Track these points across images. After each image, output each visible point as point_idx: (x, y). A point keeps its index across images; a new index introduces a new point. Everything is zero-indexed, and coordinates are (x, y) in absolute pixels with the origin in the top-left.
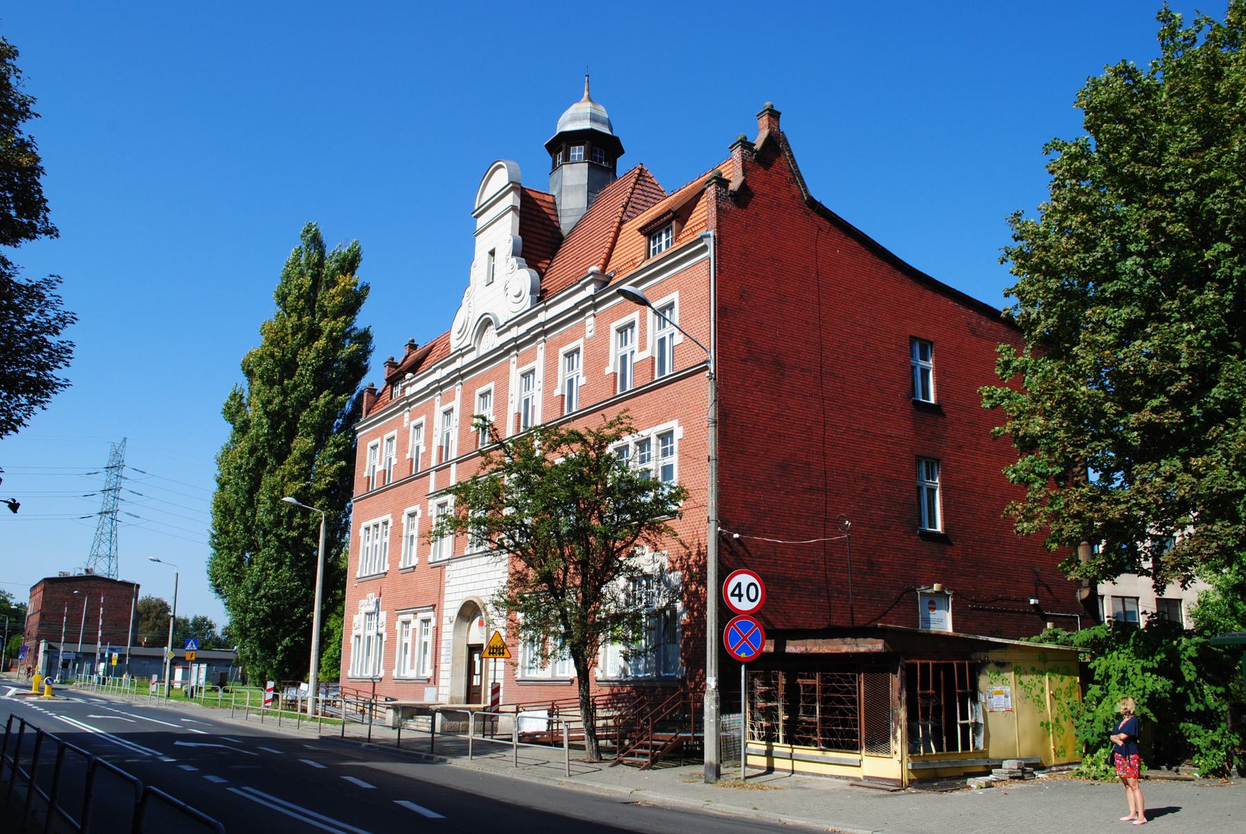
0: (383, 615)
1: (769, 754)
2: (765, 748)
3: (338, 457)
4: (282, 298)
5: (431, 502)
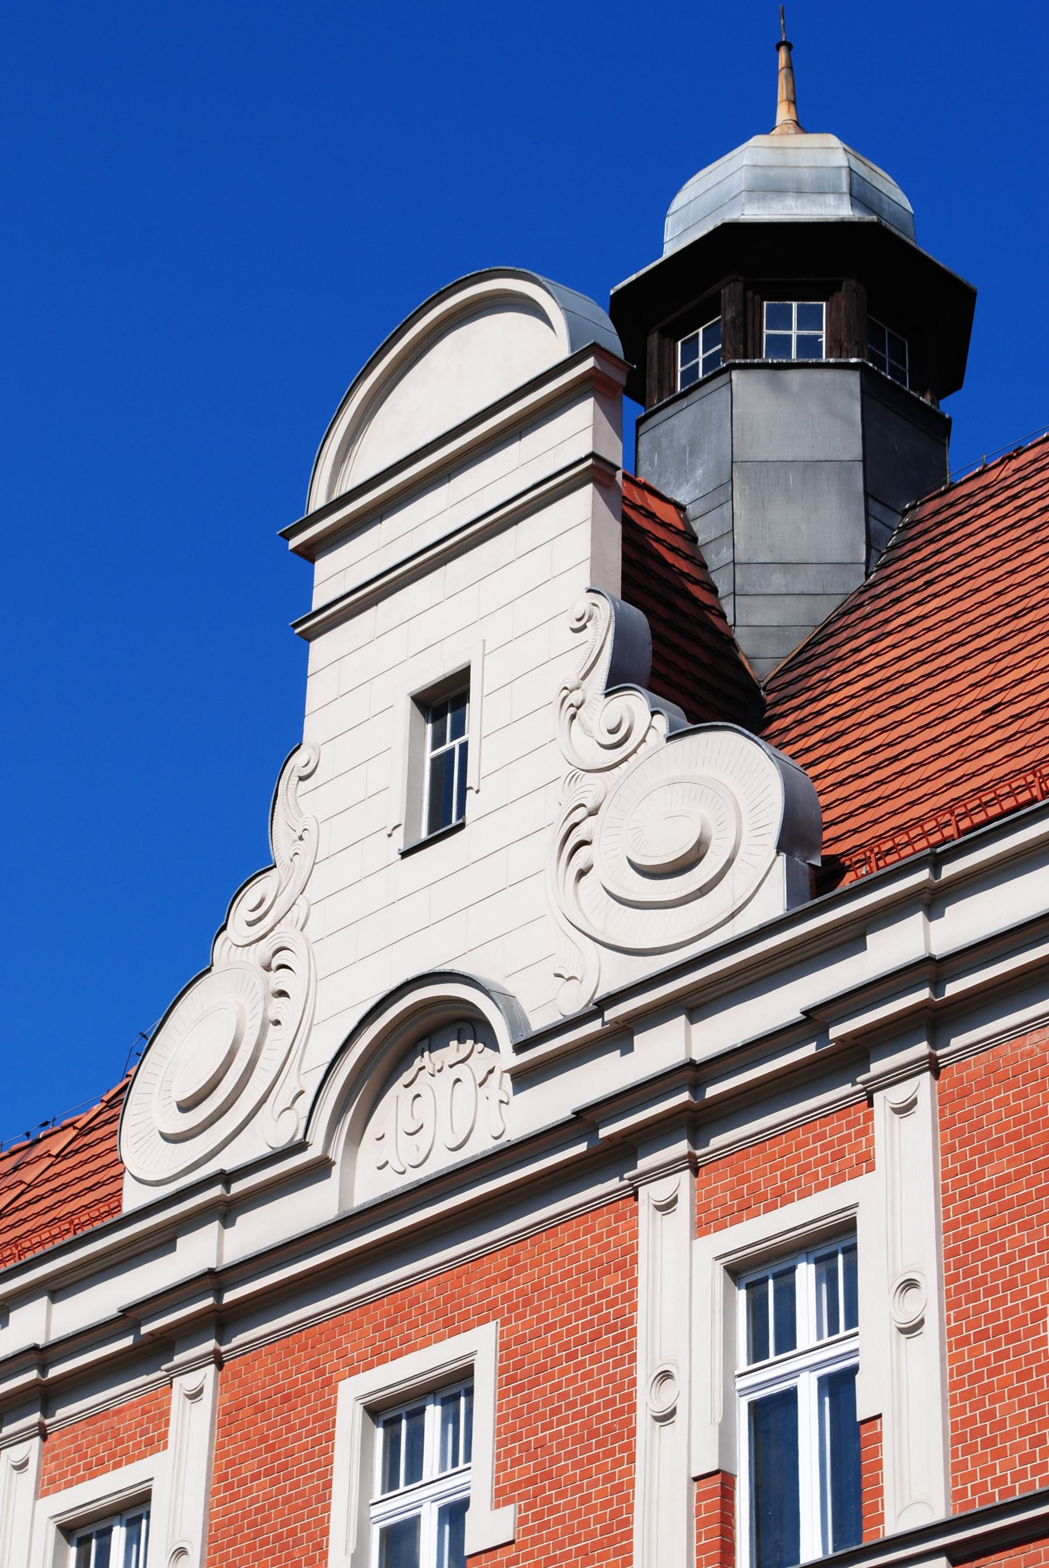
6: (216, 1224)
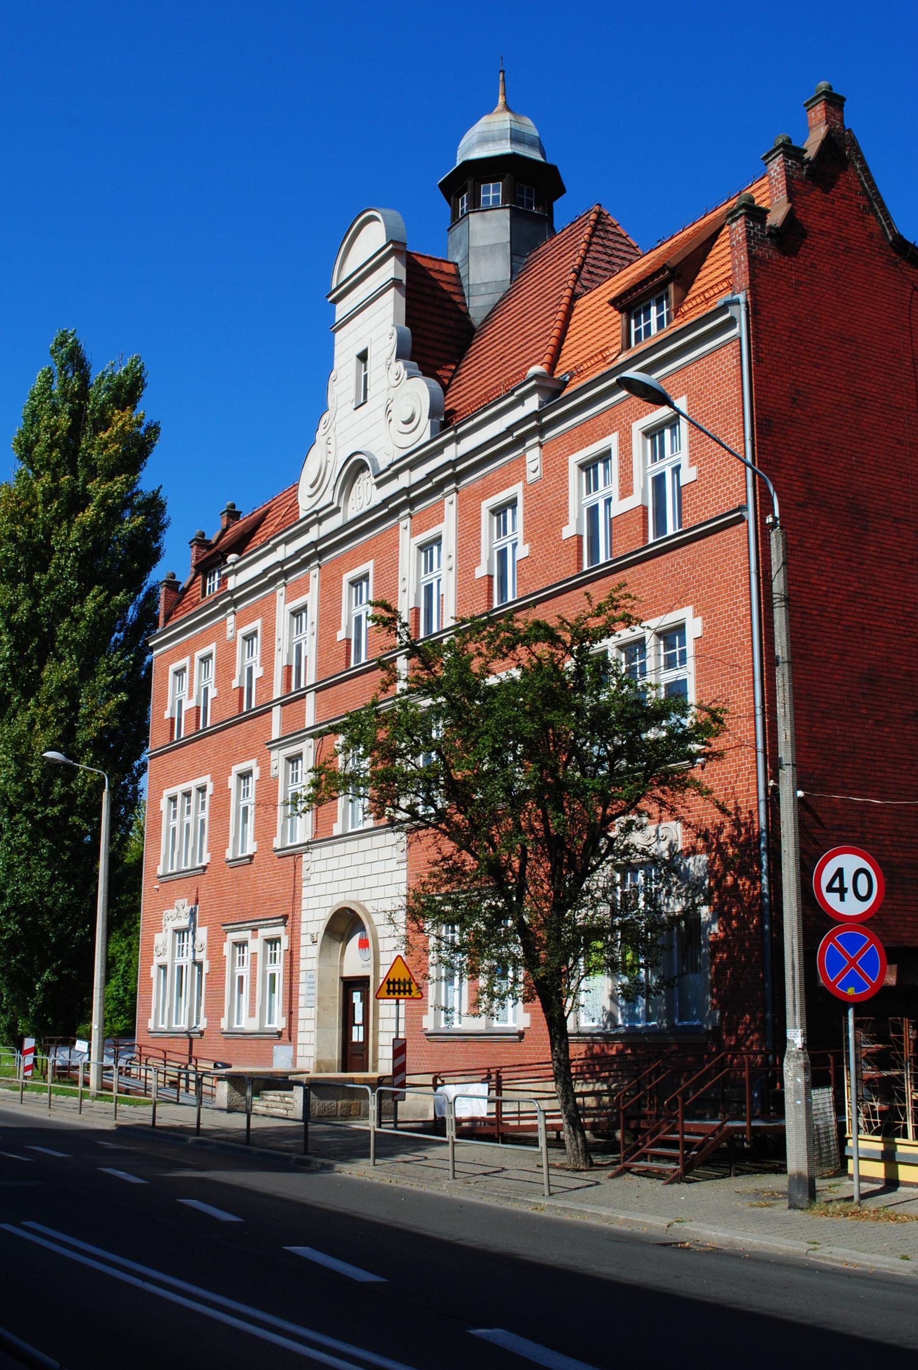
0: (202, 933)
1: (889, 1157)
2: (880, 1147)
3: (115, 687)
4: (26, 450)
5: (274, 754)
6: (454, 444)
